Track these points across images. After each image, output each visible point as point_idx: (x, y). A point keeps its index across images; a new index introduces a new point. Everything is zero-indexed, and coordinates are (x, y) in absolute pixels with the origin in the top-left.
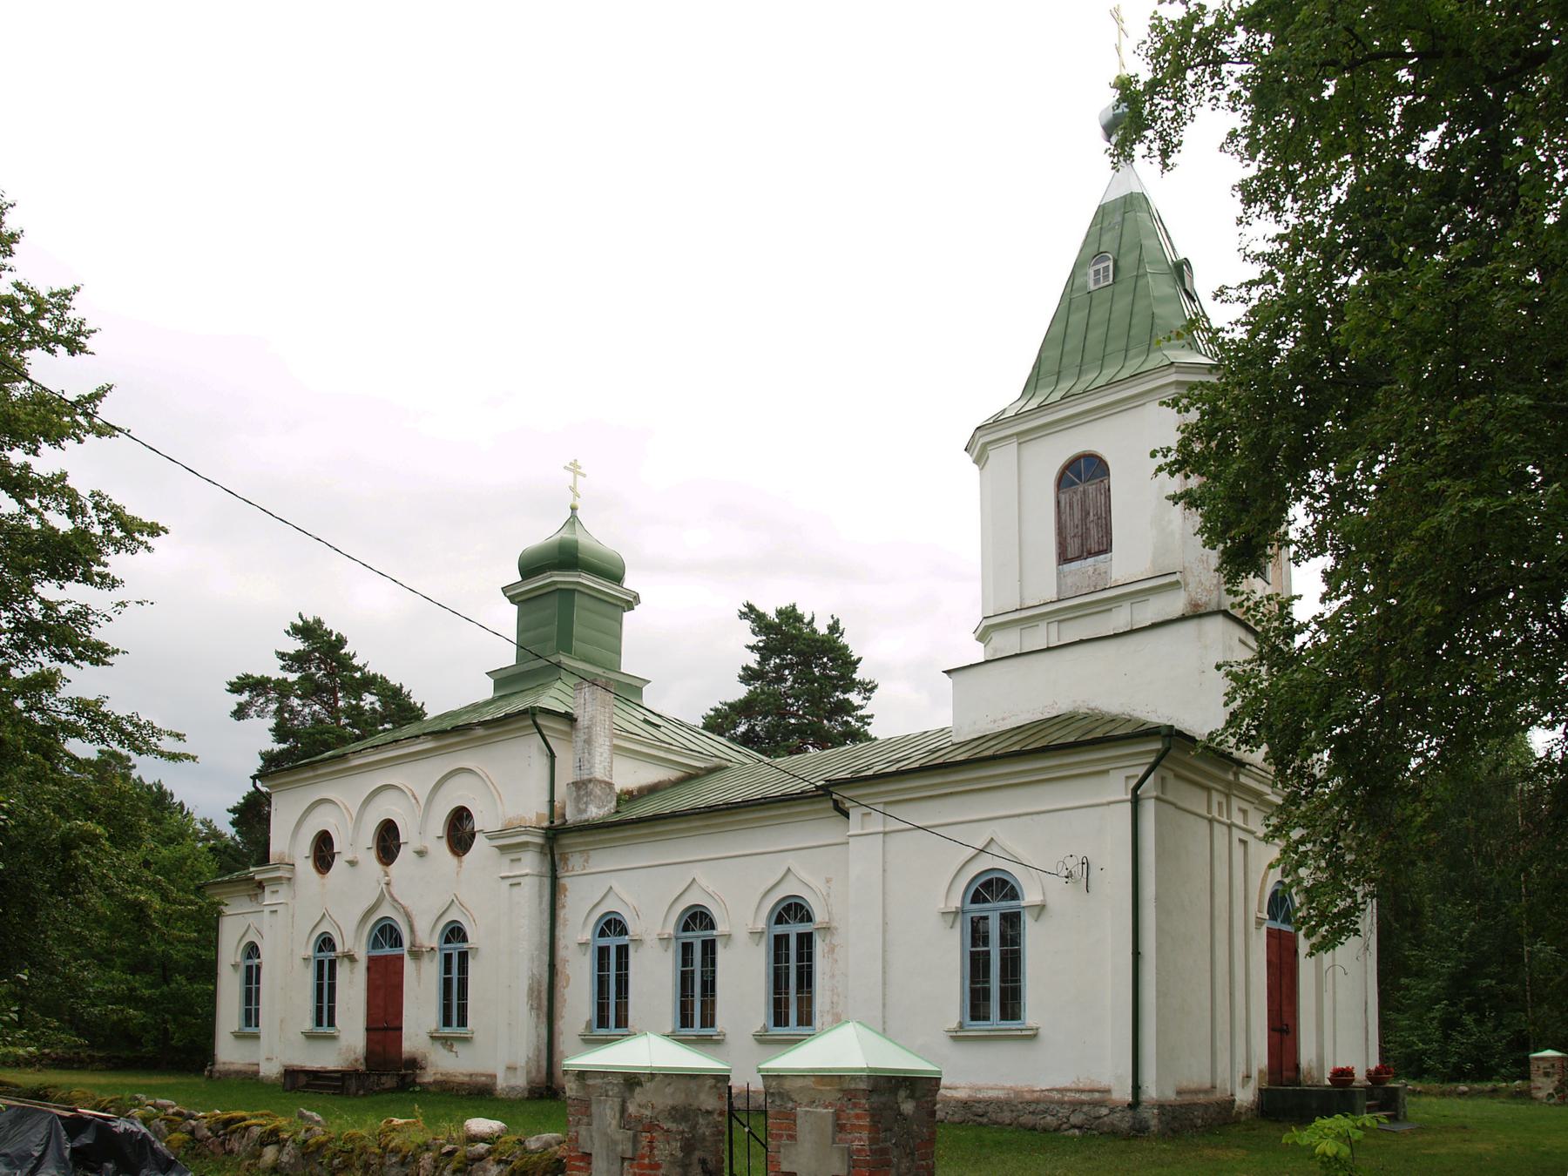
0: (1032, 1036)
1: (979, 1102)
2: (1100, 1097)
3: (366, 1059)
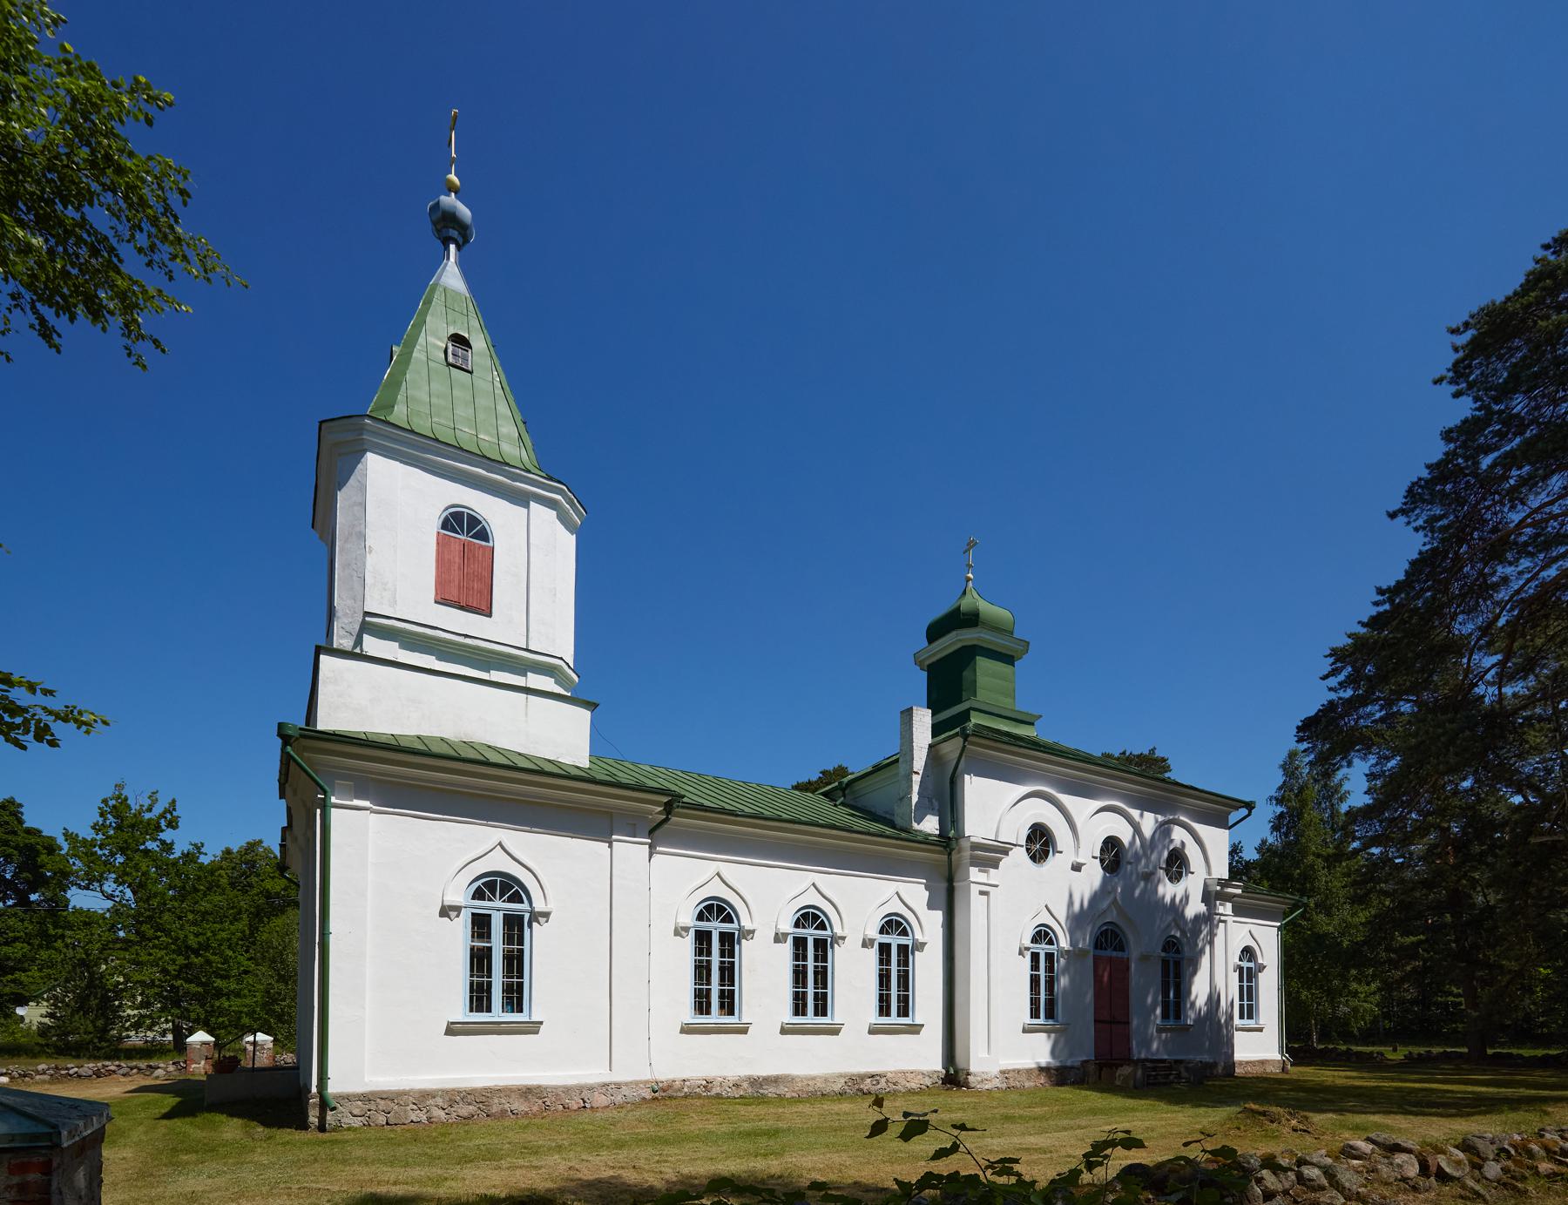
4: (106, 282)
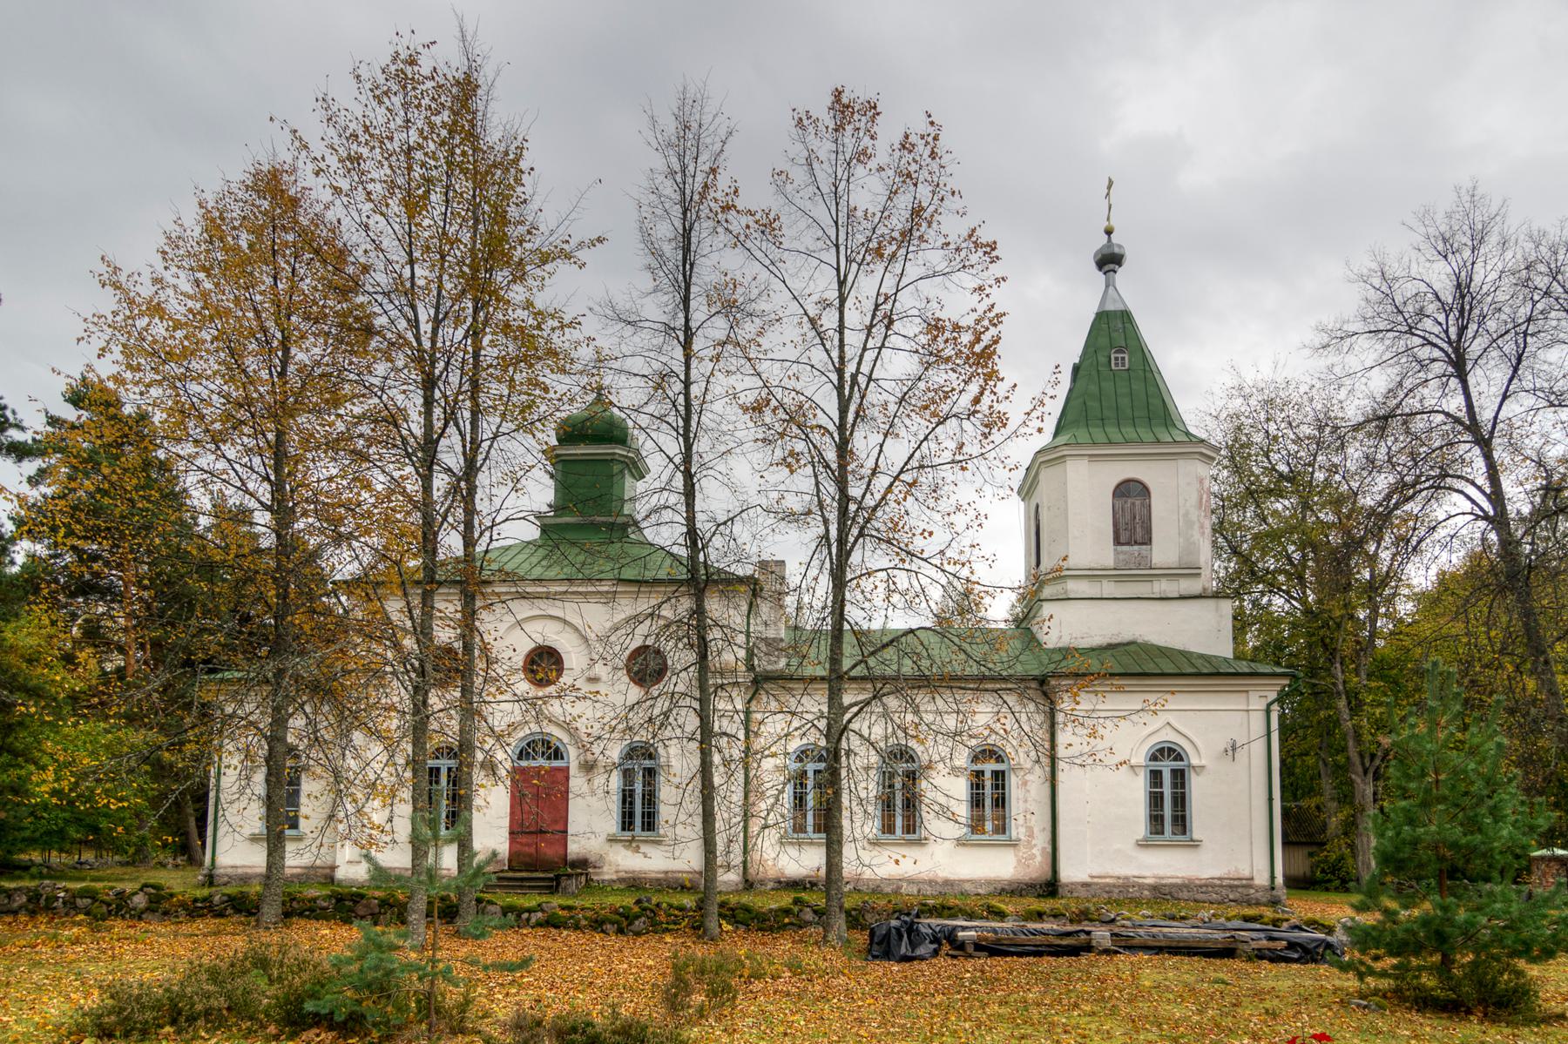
0: (1194, 845)
1: (1165, 885)
2: (1248, 883)
3: (510, 861)
4: (391, 155)
